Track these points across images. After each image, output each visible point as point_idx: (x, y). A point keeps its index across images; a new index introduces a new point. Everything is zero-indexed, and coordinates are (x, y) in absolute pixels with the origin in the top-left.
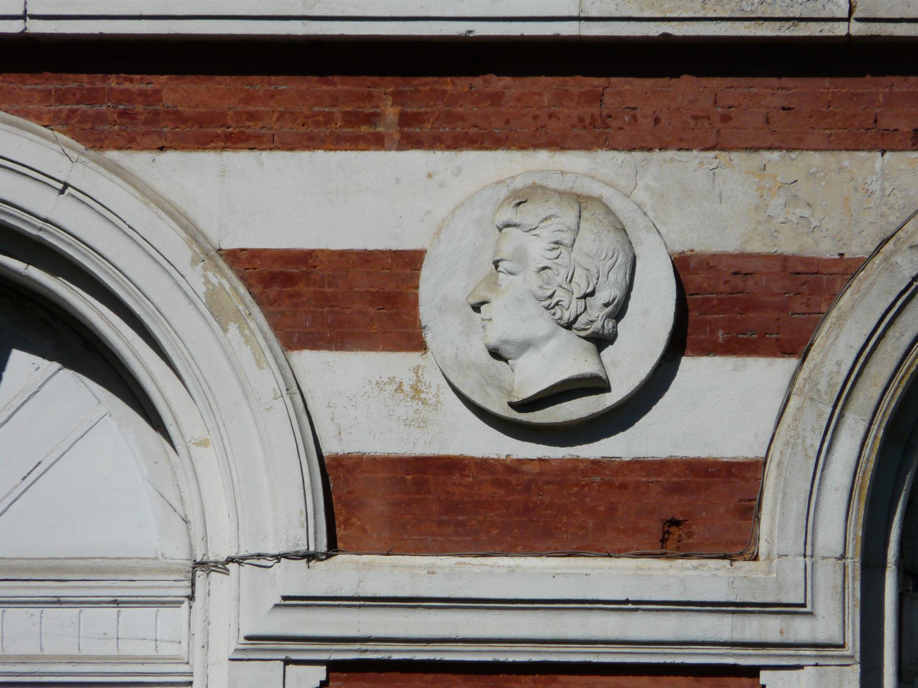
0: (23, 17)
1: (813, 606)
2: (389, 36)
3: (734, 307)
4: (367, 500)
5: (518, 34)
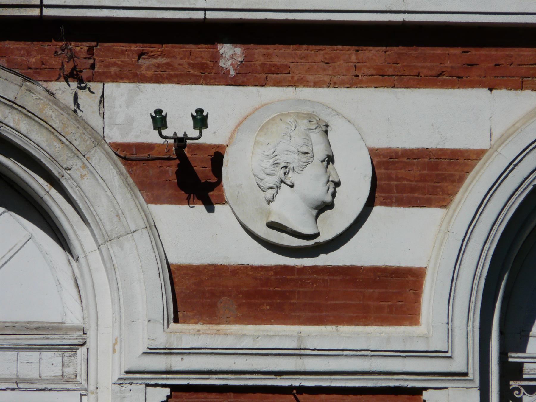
0: (41, 6)
1: (452, 352)
2: (426, 22)
3: (412, 178)
4: (196, 292)
5: (264, 18)
